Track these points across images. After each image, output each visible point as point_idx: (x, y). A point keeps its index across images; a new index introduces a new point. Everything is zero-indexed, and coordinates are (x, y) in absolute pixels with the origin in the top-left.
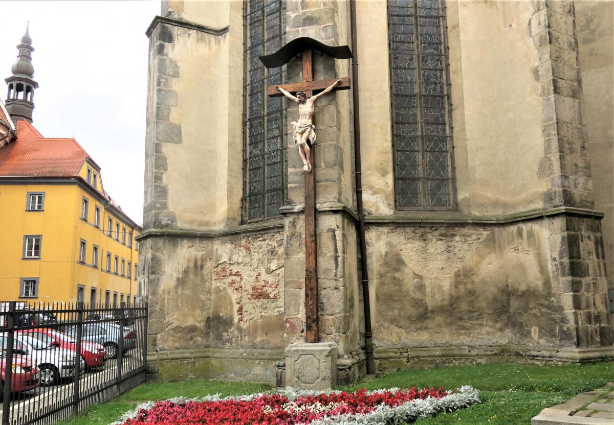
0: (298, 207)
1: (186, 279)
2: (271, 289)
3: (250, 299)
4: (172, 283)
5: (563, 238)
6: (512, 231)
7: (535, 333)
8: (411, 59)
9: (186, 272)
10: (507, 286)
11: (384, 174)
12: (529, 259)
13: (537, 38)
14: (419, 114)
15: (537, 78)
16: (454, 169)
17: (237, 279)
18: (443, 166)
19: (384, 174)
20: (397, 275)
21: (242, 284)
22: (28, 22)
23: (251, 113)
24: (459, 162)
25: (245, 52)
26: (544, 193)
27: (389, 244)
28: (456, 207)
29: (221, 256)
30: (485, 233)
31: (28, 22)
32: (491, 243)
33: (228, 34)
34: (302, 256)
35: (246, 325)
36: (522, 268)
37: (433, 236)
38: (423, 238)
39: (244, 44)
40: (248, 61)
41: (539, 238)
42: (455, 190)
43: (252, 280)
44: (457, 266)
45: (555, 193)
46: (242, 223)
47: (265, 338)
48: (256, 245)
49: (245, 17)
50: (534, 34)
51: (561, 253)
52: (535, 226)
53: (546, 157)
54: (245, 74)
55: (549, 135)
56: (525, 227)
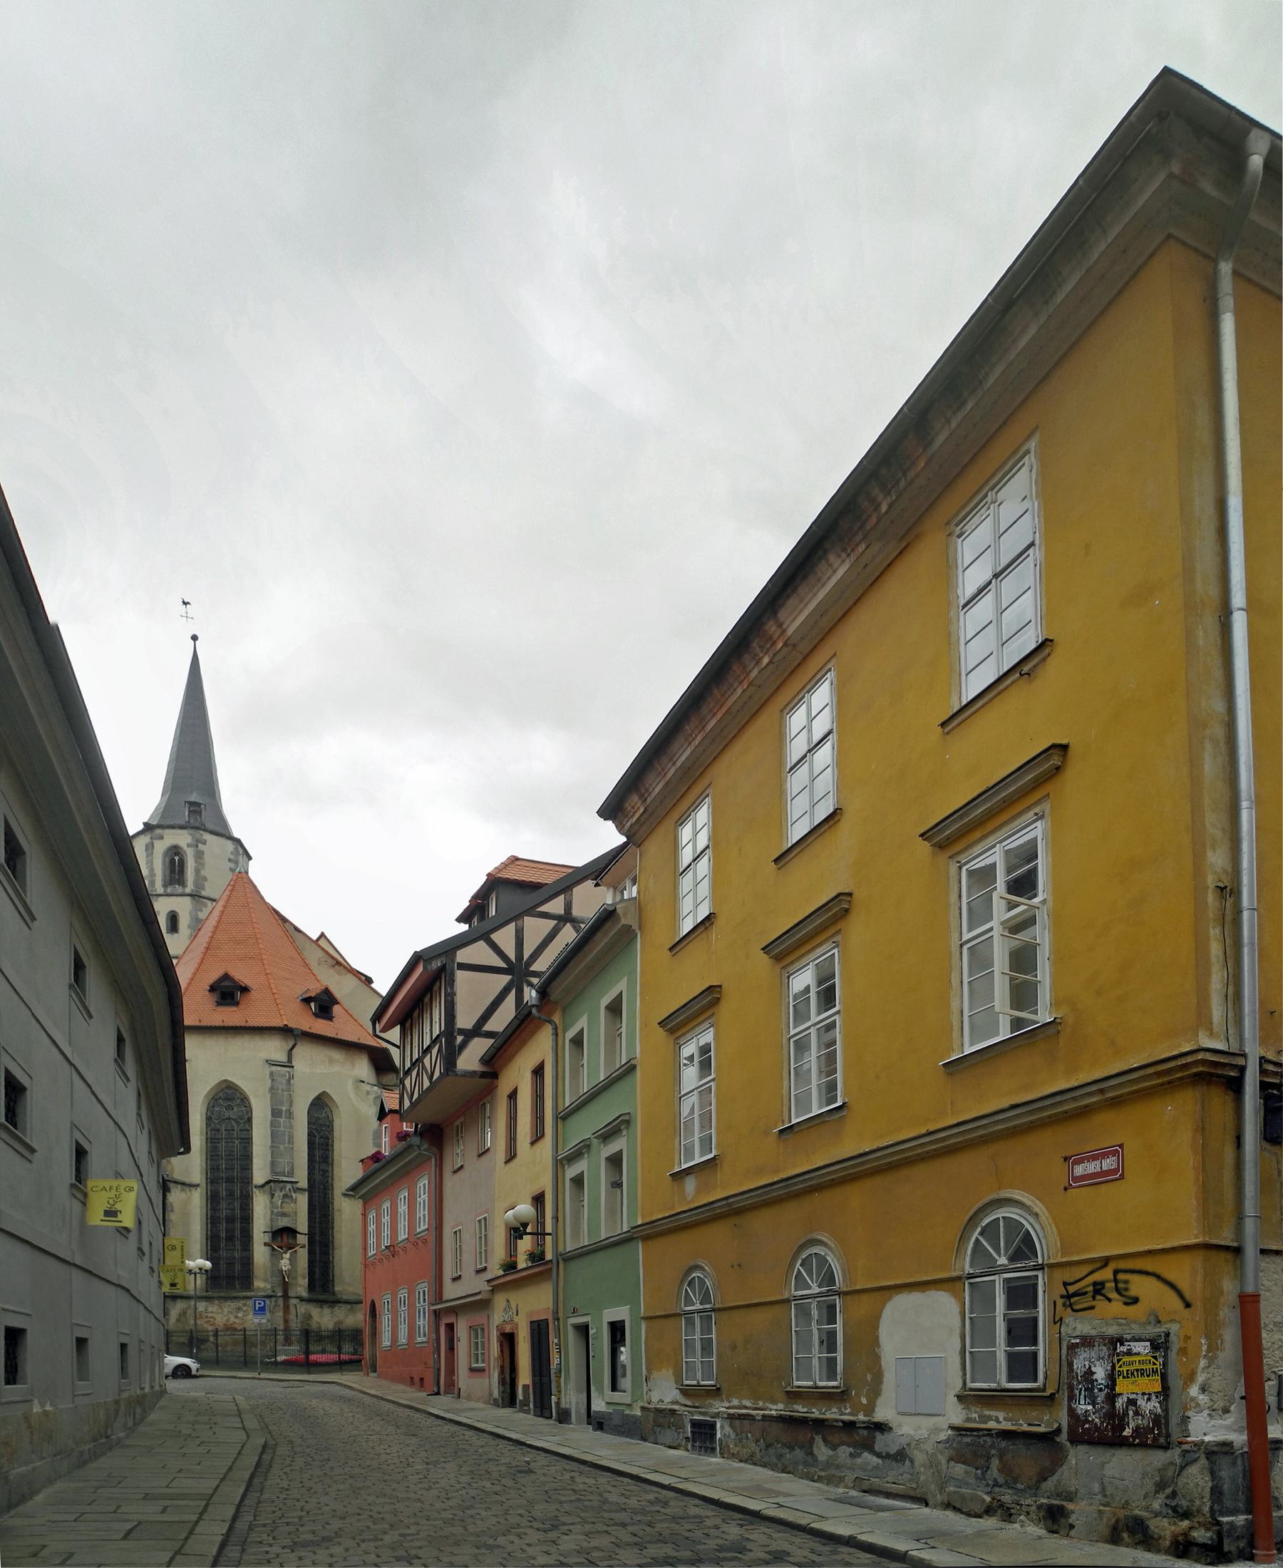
0: (280, 1294)
4: (175, 1320)
9: (180, 1315)
16: (333, 1276)
18: (328, 1274)
19: (304, 1278)
23: (211, 1233)
24: (336, 1273)
27: (306, 1309)
28: (334, 1293)
30: (349, 1306)
31: (195, 638)
32: (351, 1309)
33: (199, 1189)
34: (281, 1313)
37: (325, 1307)
38: (321, 1307)
42: (333, 1286)
44: (336, 1320)
46: (207, 1291)
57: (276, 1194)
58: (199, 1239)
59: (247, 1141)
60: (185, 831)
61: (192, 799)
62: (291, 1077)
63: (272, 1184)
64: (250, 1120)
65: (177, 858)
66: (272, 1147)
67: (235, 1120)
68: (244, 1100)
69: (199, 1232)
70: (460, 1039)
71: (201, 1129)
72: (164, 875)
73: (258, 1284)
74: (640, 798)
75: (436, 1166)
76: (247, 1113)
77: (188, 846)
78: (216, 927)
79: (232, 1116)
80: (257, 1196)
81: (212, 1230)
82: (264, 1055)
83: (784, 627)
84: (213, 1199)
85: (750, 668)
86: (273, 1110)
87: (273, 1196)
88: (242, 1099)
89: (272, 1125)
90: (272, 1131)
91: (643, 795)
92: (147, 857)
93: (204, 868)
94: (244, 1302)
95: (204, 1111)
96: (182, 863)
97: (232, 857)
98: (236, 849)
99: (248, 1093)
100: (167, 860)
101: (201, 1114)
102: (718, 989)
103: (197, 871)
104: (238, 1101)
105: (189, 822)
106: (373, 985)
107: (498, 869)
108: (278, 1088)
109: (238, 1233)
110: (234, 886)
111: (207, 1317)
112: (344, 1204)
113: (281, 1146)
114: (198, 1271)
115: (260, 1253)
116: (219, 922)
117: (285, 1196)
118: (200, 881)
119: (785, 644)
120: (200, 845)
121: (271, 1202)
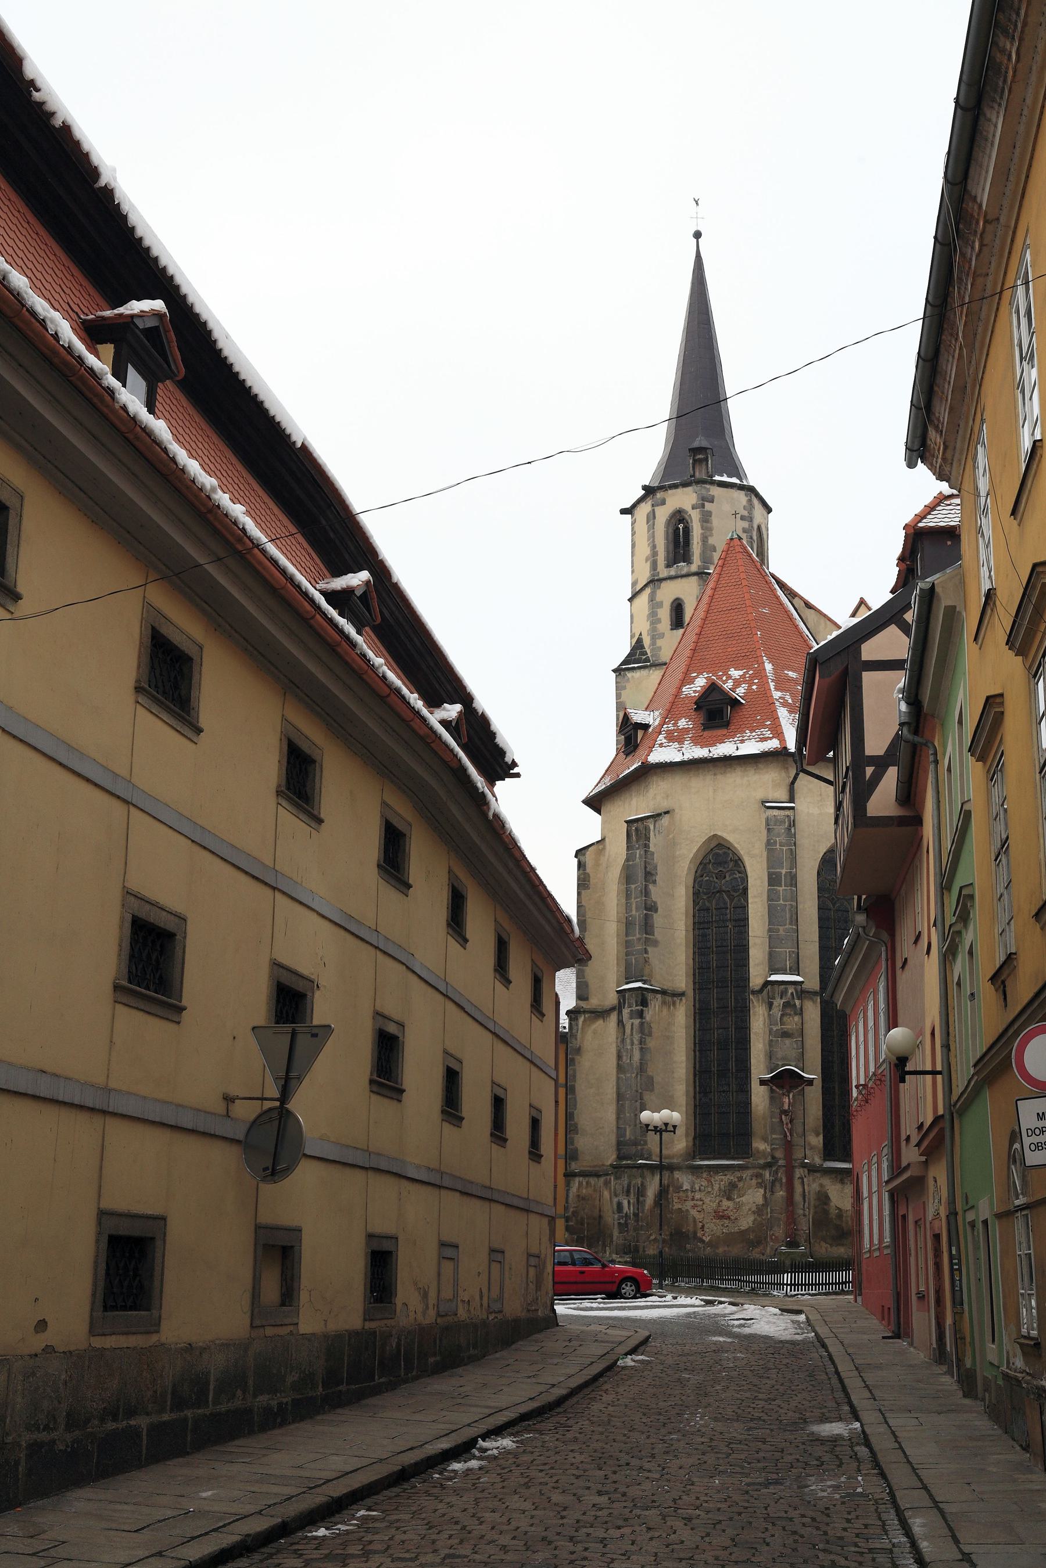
1: (788, 1262)
8: (832, 1044)
11: (817, 1135)
14: (837, 1088)
20: (825, 1207)
21: (704, 1207)
22: (698, 235)
23: (700, 1066)
25: (695, 1013)
27: (821, 1185)
31: (698, 235)
35: (708, 1238)
39: (694, 1006)
40: (697, 1021)
43: (714, 1205)
47: (726, 1248)
49: (694, 983)
54: (695, 1032)
57: (776, 1003)
58: (684, 1077)
59: (742, 923)
60: (689, 489)
61: (696, 444)
62: (793, 824)
64: (745, 890)
65: (681, 526)
66: (770, 930)
68: (738, 863)
69: (684, 1065)
70: (869, 771)
71: (687, 911)
72: (667, 551)
73: (760, 1145)
74: (937, 431)
75: (887, 960)
77: (693, 509)
78: (705, 620)
79: (724, 888)
80: (754, 1007)
82: (760, 795)
83: (979, 200)
84: (702, 1015)
85: (969, 254)
86: (770, 875)
87: (770, 1005)
88: (736, 861)
89: (770, 899)
90: (769, 906)
91: (938, 426)
92: (648, 531)
93: (711, 535)
94: (738, 1174)
95: (691, 884)
96: (687, 531)
97: (746, 513)
98: (750, 501)
99: (742, 852)
100: (671, 531)
101: (687, 887)
102: (998, 700)
103: (704, 539)
104: (731, 864)
105: (693, 476)
107: (921, 517)
108: (775, 842)
109: (732, 1065)
110: (725, 559)
111: (693, 1199)
113: (781, 928)
114: (664, 1128)
115: (759, 1095)
116: (707, 612)
117: (786, 1005)
119: (986, 222)
120: (706, 504)
121: (769, 1015)
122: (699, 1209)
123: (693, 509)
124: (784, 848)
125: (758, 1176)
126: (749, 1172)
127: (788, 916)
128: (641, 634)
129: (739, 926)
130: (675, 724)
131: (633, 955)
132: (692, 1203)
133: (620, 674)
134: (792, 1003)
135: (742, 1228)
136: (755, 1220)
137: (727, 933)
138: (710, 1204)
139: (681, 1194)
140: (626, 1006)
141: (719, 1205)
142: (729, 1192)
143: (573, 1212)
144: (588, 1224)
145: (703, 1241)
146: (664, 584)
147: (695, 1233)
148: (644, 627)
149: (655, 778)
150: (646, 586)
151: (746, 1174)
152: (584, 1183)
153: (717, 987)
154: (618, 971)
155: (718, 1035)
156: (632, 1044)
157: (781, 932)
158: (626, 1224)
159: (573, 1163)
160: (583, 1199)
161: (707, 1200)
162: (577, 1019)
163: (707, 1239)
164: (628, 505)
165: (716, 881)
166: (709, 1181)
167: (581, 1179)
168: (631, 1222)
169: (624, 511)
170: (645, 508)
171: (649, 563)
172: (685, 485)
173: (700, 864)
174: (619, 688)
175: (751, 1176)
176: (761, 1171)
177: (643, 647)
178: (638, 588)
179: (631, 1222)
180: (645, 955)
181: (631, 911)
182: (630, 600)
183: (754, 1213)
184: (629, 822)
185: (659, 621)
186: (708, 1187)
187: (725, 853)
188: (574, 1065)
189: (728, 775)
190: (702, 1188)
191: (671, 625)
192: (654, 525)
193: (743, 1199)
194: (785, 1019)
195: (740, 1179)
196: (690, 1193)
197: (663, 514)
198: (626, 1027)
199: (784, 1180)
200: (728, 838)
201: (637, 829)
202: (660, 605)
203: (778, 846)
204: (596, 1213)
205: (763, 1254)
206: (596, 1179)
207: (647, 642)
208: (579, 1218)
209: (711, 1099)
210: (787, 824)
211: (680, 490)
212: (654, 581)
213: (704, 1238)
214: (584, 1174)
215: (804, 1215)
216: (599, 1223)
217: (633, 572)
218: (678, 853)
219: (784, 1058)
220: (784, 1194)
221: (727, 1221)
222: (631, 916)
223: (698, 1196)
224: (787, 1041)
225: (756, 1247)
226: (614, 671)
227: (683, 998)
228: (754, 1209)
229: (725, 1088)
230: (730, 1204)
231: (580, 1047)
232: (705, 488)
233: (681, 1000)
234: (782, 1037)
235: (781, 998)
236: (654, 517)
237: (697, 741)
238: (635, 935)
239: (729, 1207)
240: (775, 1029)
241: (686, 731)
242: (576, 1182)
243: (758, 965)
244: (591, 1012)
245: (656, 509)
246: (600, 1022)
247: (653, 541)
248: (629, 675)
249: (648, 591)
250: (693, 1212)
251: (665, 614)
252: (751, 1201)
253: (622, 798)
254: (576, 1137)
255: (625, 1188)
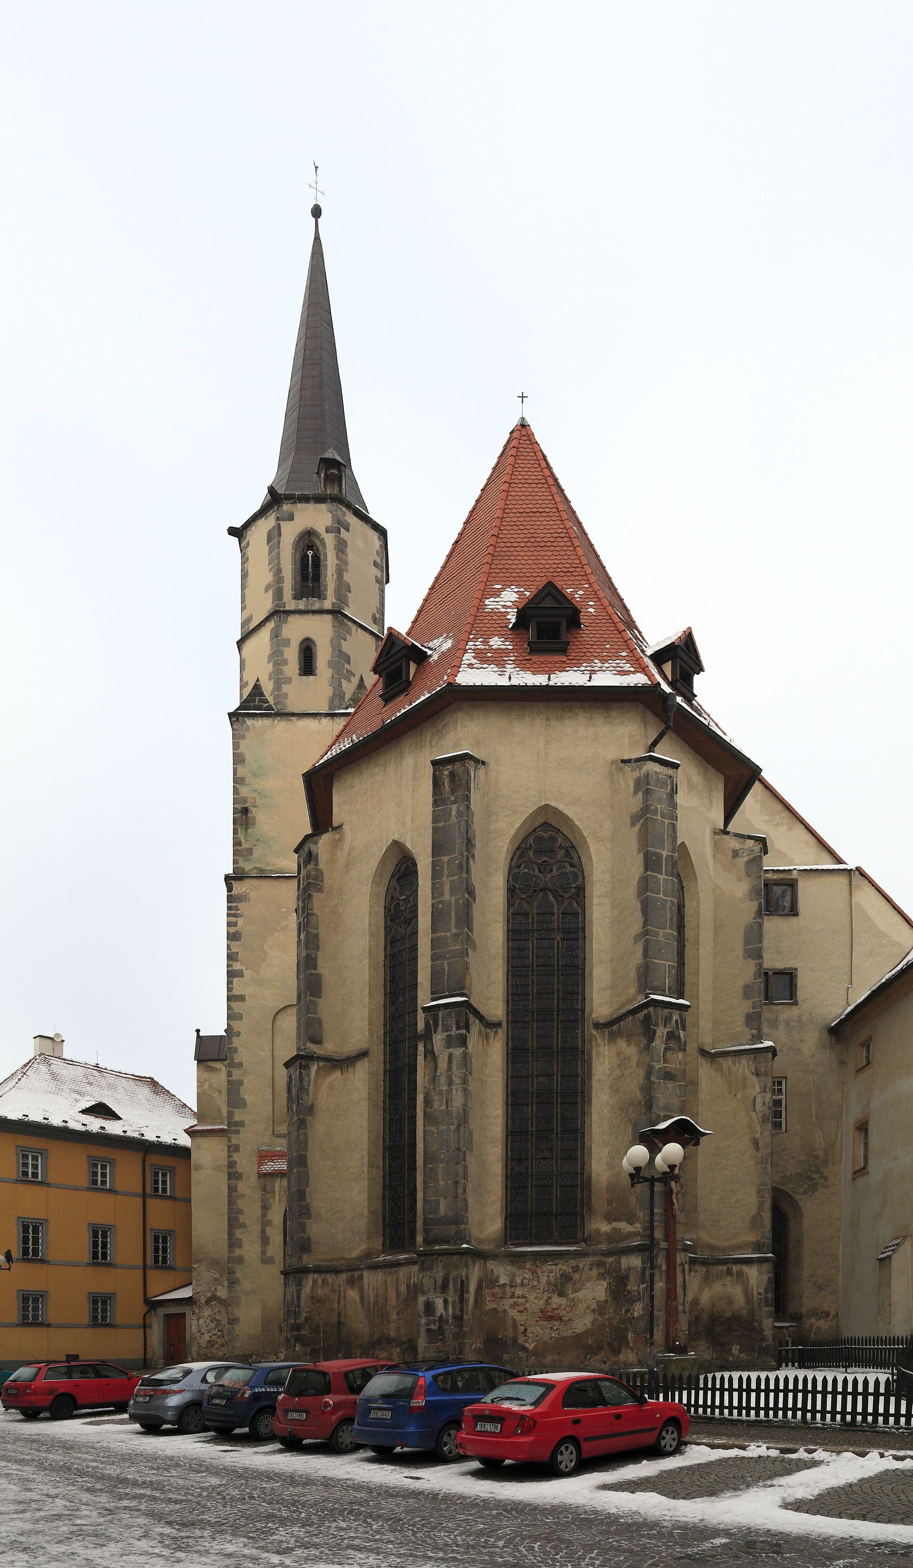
2: (564, 1312)
3: (537, 1321)
5: (769, 1279)
6: (722, 1270)
7: (736, 1350)
10: (713, 1314)
12: (737, 1293)
13: (760, 1115)
15: (757, 1149)
17: (523, 1301)
21: (528, 1305)
22: (317, 212)
26: (753, 1242)
29: (499, 1276)
31: (317, 212)
35: (533, 1345)
36: (730, 1301)
41: (747, 1278)
43: (541, 1303)
45: (764, 1243)
47: (556, 1357)
48: (544, 1268)
50: (757, 1110)
51: (766, 1291)
52: (745, 1268)
53: (758, 1214)
55: (763, 1197)
56: (735, 1268)
60: (323, 507)
63: (651, 1009)
67: (555, 893)
76: (576, 875)
77: (327, 532)
80: (598, 1046)
81: (390, 1166)
82: (614, 753)
92: (270, 552)
94: (573, 1263)
96: (317, 560)
100: (298, 557)
104: (561, 854)
106: (216, 1027)
111: (513, 1296)
112: (701, 1071)
113: (661, 932)
118: (343, 589)
120: (342, 530)
122: (521, 1308)
123: (327, 532)
124: (666, 821)
125: (599, 1264)
126: (588, 1260)
127: (668, 916)
128: (258, 680)
129: (570, 939)
130: (485, 642)
131: (445, 958)
132: (511, 1301)
133: (238, 720)
134: (677, 1035)
135: (577, 1331)
136: (595, 1320)
137: (553, 948)
138: (535, 1302)
139: (497, 1290)
140: (440, 1028)
141: (547, 1302)
142: (561, 1286)
143: (307, 1318)
144: (324, 1332)
145: (526, 1350)
146: (292, 619)
147: (515, 1339)
148: (262, 671)
149: (460, 715)
150: (267, 619)
151: (585, 1263)
152: (320, 1281)
153: (537, 1021)
154: (370, 1004)
155: (538, 1084)
156: (450, 1083)
157: (661, 938)
158: (441, 1331)
159: (305, 1256)
160: (319, 1301)
161: (531, 1297)
162: (308, 1067)
163: (531, 1346)
164: (238, 524)
165: (539, 875)
166: (534, 1272)
167: (316, 1276)
168: (450, 1328)
169: (232, 531)
170: (267, 524)
171: (270, 593)
172: (319, 499)
173: (518, 849)
174: (237, 738)
175: (592, 1265)
176: (603, 1259)
177: (262, 694)
178: (252, 626)
179: (450, 1328)
180: (466, 959)
181: (443, 894)
182: (240, 644)
183: (594, 1311)
184: (435, 763)
185: (285, 662)
186: (532, 1280)
187: (551, 837)
188: (306, 1129)
189: (567, 722)
190: (526, 1281)
191: (300, 669)
192: (279, 543)
193: (580, 1294)
194: (669, 1054)
195: (576, 1269)
196: (508, 1288)
197: (290, 532)
198: (440, 1060)
199: (664, 1268)
200: (566, 812)
201: (452, 775)
202: (287, 643)
203: (659, 817)
204: (334, 1319)
205: (605, 1363)
206: (333, 1276)
207: (268, 688)
208: (313, 1326)
209: (526, 1169)
210: (669, 787)
211: (311, 506)
212: (278, 613)
213: (527, 1345)
214: (318, 1270)
215: (684, 1312)
216: (339, 1331)
217: (243, 608)
218: (493, 827)
219: (665, 1108)
220: (664, 1285)
221: (557, 1323)
222: (441, 902)
223: (519, 1291)
224: (670, 1085)
225: (596, 1353)
226: (231, 715)
227: (499, 1030)
228: (594, 1306)
229: (547, 1154)
230: (563, 1301)
231: (313, 1104)
232: (341, 509)
233: (496, 1032)
234: (664, 1079)
235: (665, 1026)
236: (280, 535)
237: (523, 665)
238: (449, 930)
239: (560, 1306)
240: (657, 1067)
241: (506, 652)
242: (309, 1282)
243: (604, 989)
244: (327, 1059)
245: (282, 524)
246: (337, 1074)
247: (279, 563)
248: (249, 722)
249: (271, 625)
250: (513, 1313)
251: (292, 655)
252: (590, 1296)
253: (381, 762)
254: (309, 1223)
255: (439, 1283)
